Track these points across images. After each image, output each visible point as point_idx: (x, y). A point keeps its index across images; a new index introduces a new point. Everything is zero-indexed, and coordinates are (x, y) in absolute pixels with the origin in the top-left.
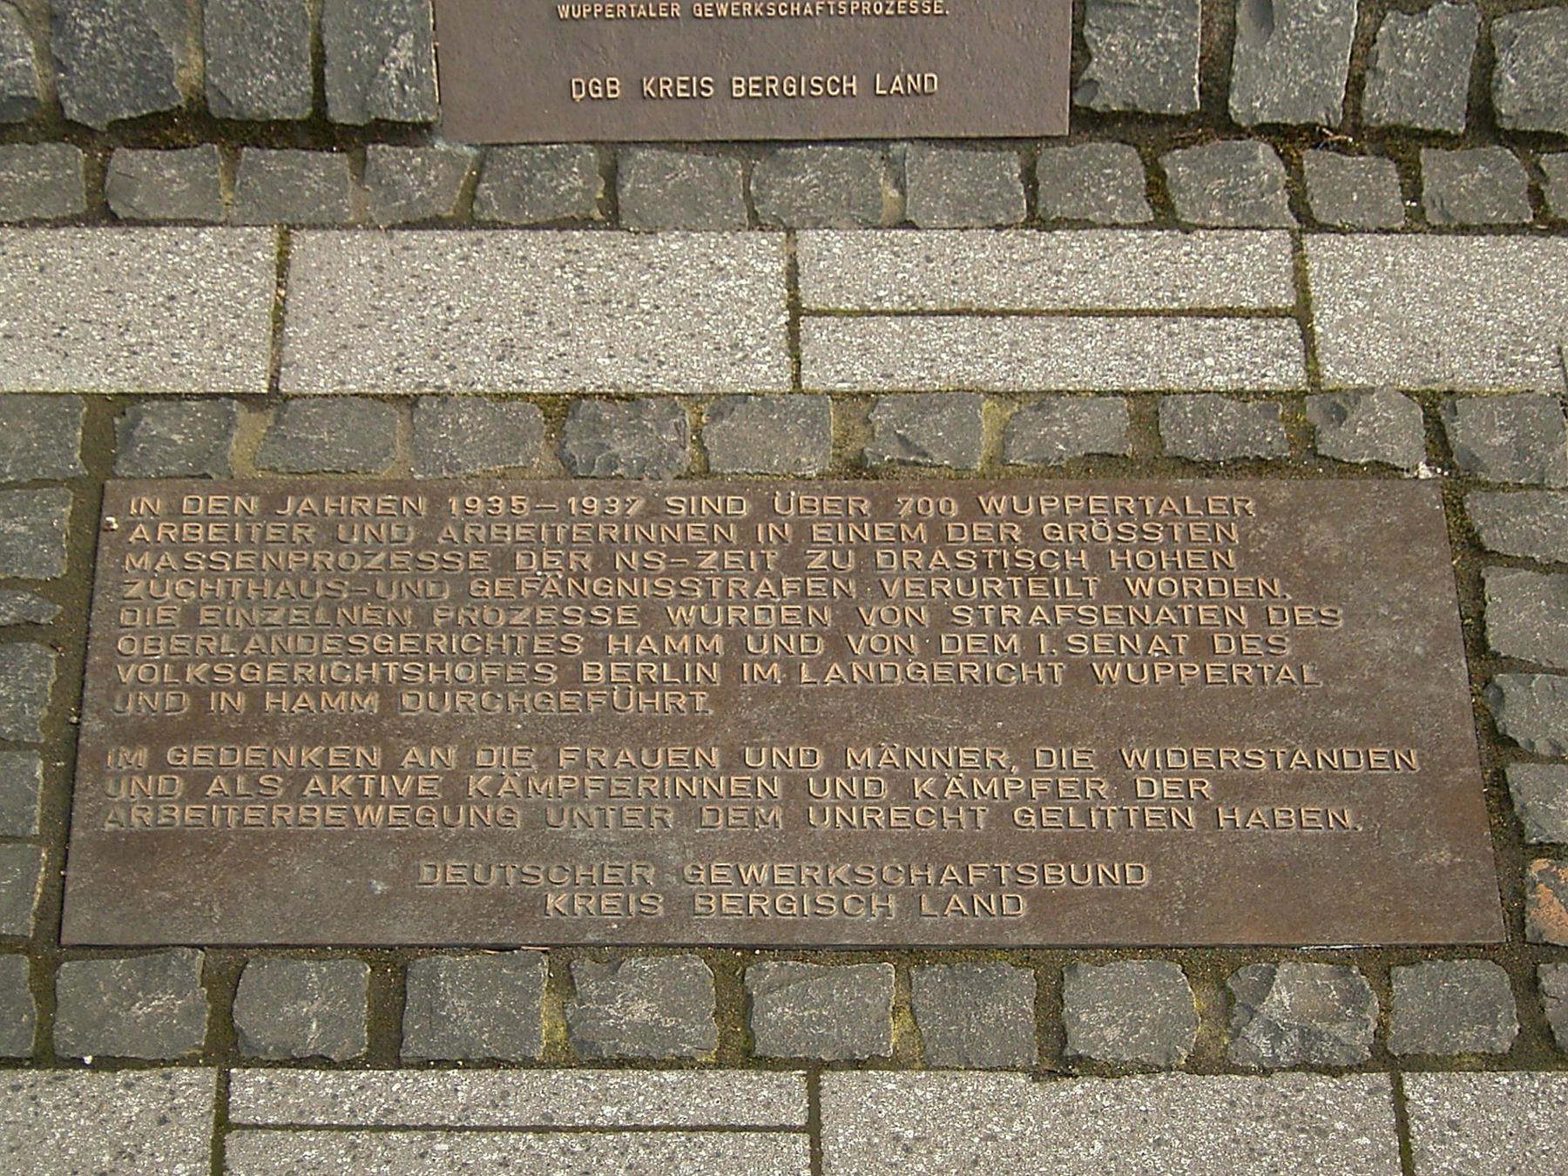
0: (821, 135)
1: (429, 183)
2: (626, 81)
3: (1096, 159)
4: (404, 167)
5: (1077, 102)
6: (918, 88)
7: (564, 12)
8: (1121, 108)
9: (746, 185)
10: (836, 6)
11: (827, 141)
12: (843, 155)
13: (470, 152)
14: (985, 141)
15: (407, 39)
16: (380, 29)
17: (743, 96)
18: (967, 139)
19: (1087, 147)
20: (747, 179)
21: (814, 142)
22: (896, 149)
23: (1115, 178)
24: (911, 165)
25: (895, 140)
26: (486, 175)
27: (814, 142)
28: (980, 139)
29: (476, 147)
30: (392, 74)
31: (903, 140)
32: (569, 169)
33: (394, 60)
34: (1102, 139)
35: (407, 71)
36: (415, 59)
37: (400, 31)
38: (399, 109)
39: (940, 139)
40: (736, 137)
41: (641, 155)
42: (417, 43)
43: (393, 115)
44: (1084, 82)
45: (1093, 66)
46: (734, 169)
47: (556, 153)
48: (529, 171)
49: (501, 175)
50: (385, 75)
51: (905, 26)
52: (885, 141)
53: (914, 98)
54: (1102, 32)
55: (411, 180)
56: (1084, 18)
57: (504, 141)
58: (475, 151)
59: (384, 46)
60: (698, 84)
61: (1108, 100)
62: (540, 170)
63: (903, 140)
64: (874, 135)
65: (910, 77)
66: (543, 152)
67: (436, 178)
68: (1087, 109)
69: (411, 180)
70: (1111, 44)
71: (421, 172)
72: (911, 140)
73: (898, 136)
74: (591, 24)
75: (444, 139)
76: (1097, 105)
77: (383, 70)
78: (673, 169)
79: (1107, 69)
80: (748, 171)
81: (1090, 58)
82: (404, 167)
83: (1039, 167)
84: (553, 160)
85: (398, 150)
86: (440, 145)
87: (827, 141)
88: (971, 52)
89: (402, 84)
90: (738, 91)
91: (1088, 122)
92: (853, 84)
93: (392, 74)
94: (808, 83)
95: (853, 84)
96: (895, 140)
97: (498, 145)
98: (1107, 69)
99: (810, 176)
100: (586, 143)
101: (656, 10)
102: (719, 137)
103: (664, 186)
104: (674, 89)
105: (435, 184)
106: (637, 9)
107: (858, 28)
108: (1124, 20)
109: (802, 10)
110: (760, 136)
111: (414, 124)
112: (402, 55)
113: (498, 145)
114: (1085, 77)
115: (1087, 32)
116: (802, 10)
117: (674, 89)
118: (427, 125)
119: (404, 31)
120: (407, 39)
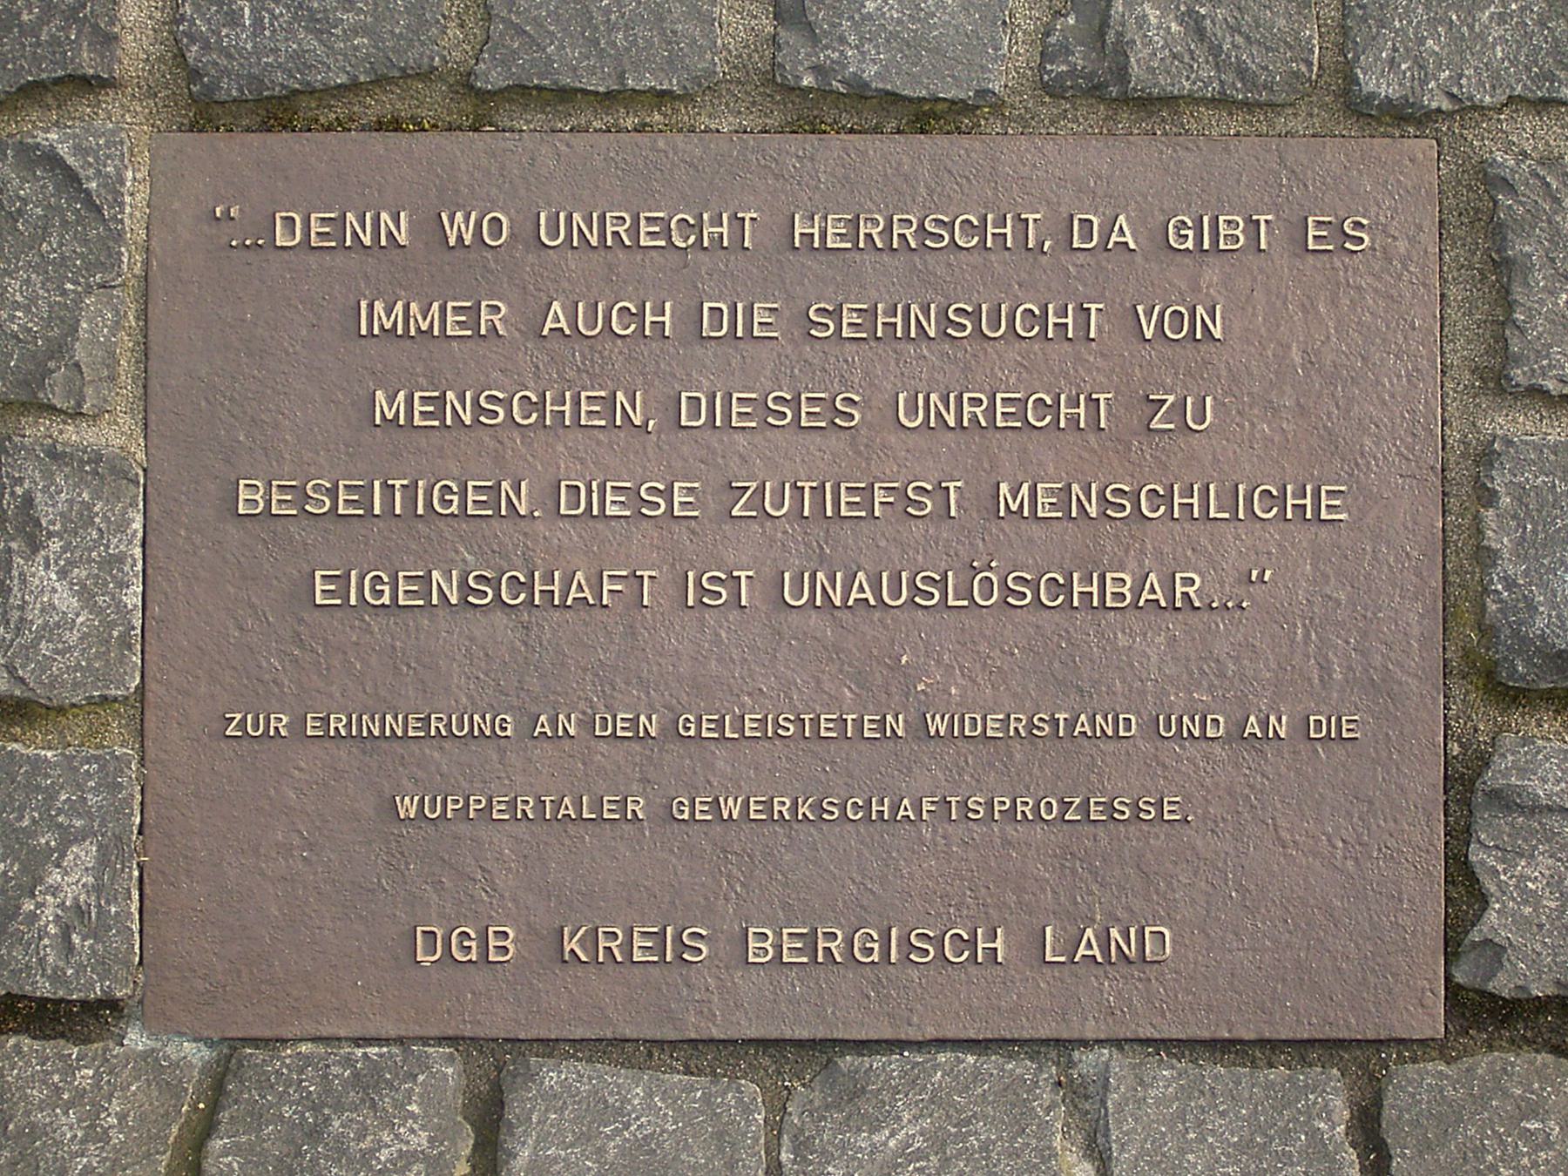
0: (931, 1032)
1: (105, 1137)
2: (529, 931)
3: (1506, 1094)
4: (58, 1090)
5: (1459, 978)
6: (1132, 953)
7: (408, 807)
8: (1551, 991)
9: (773, 1149)
10: (964, 804)
11: (942, 1043)
12: (977, 1076)
13: (195, 1053)
14: (1271, 1048)
15: (84, 854)
16: (30, 833)
17: (762, 970)
18: (1233, 1042)
19: (1484, 1063)
20: (775, 1129)
21: (918, 1045)
22: (1087, 1061)
23: (1548, 1144)
24: (1120, 1108)
25: (1084, 1043)
26: (224, 1116)
27: (918, 1045)
28: (1262, 1043)
29: (209, 1043)
30: (48, 914)
31: (1100, 1042)
32: (400, 1106)
33: (55, 890)
34: (1515, 1044)
35: (80, 911)
36: (98, 889)
37: (69, 838)
38: (57, 977)
39: (1179, 1042)
40: (752, 1033)
41: (552, 1077)
42: (103, 861)
43: (44, 989)
44: (1474, 945)
45: (1492, 917)
46: (747, 1110)
47: (375, 1067)
48: (315, 1109)
49: (258, 1117)
50: (33, 917)
51: (1104, 842)
52: (1063, 1045)
53: (1125, 969)
54: (1509, 855)
55: (69, 1124)
56: (1468, 830)
57: (268, 1034)
58: (206, 1053)
59: (34, 867)
60: (678, 937)
61: (1527, 973)
62: (339, 1108)
63: (1100, 1042)
64: (1044, 1033)
65: (1114, 933)
66: (348, 1061)
67: (122, 1117)
68: (1482, 993)
69: (69, 1124)
70: (1523, 878)
71: (90, 1104)
72: (1118, 1043)
73: (1089, 1035)
74: (463, 828)
75: (145, 1026)
76: (1502, 985)
77: (29, 906)
78: (620, 1112)
79: (1522, 924)
80: (778, 1106)
81: (1484, 901)
82: (58, 1090)
83: (1388, 1113)
84: (368, 1082)
85: (49, 1048)
86: (136, 1039)
87: (942, 1043)
88: (1240, 888)
89: (66, 937)
90: (759, 950)
91: (1481, 1013)
92: (999, 944)
93: (48, 914)
94: (905, 941)
95: (999, 944)
96: (1084, 1043)
97: (255, 1042)
98: (1522, 924)
99: (907, 1130)
100: (441, 1040)
101: (598, 805)
102: (716, 1033)
103: (601, 1151)
104: (635, 230)
105: (117, 1138)
106: (557, 804)
107: (1007, 843)
108: (1550, 836)
109: (895, 808)
110: (804, 1034)
111: (84, 1003)
112: (72, 878)
113: (255, 1042)
114: (1475, 936)
115: (1476, 855)
116: (895, 808)
117: (635, 230)
118: (113, 1005)
119: (80, 837)
120: (84, 854)
